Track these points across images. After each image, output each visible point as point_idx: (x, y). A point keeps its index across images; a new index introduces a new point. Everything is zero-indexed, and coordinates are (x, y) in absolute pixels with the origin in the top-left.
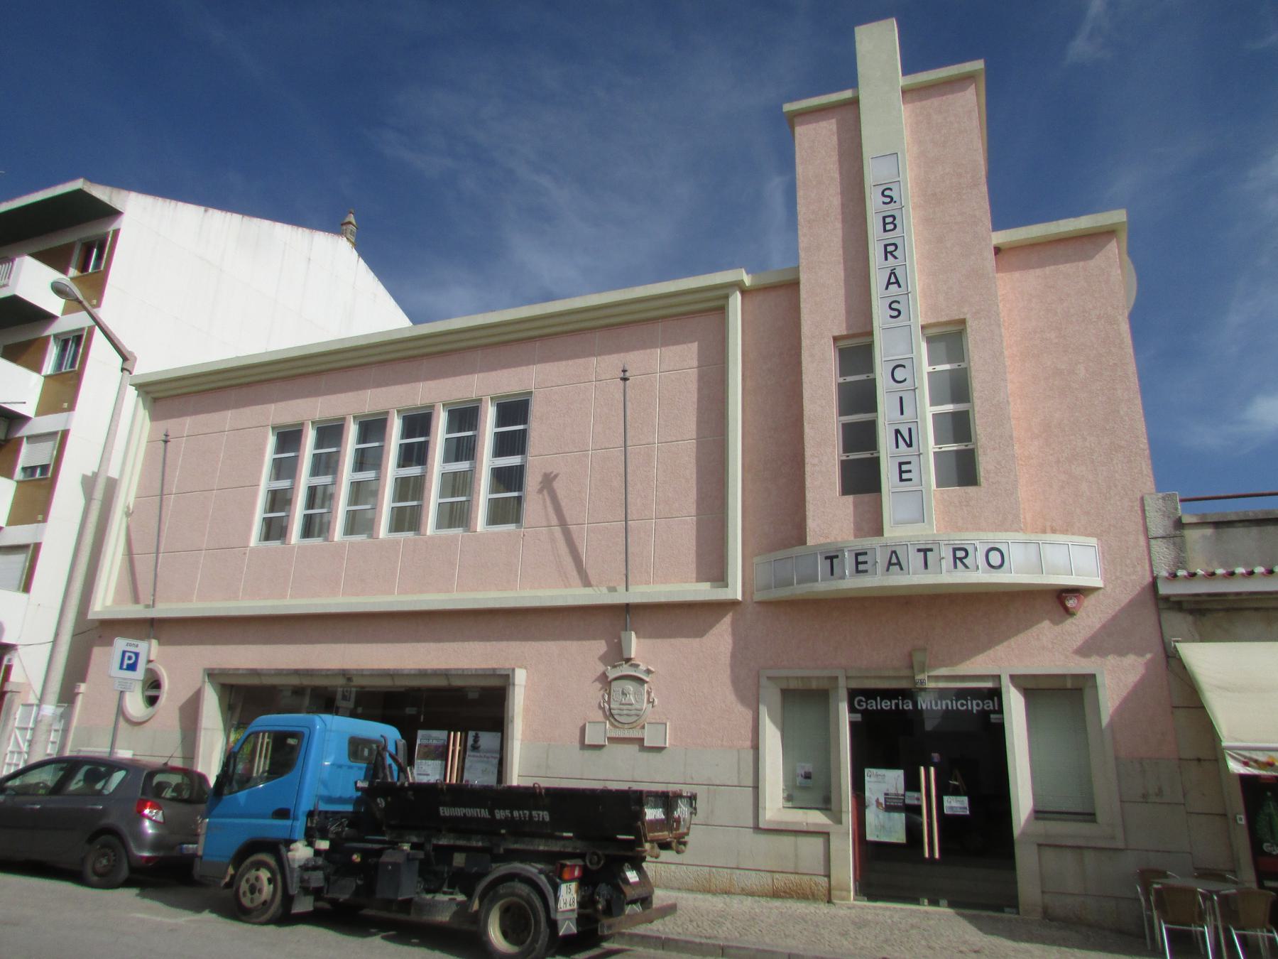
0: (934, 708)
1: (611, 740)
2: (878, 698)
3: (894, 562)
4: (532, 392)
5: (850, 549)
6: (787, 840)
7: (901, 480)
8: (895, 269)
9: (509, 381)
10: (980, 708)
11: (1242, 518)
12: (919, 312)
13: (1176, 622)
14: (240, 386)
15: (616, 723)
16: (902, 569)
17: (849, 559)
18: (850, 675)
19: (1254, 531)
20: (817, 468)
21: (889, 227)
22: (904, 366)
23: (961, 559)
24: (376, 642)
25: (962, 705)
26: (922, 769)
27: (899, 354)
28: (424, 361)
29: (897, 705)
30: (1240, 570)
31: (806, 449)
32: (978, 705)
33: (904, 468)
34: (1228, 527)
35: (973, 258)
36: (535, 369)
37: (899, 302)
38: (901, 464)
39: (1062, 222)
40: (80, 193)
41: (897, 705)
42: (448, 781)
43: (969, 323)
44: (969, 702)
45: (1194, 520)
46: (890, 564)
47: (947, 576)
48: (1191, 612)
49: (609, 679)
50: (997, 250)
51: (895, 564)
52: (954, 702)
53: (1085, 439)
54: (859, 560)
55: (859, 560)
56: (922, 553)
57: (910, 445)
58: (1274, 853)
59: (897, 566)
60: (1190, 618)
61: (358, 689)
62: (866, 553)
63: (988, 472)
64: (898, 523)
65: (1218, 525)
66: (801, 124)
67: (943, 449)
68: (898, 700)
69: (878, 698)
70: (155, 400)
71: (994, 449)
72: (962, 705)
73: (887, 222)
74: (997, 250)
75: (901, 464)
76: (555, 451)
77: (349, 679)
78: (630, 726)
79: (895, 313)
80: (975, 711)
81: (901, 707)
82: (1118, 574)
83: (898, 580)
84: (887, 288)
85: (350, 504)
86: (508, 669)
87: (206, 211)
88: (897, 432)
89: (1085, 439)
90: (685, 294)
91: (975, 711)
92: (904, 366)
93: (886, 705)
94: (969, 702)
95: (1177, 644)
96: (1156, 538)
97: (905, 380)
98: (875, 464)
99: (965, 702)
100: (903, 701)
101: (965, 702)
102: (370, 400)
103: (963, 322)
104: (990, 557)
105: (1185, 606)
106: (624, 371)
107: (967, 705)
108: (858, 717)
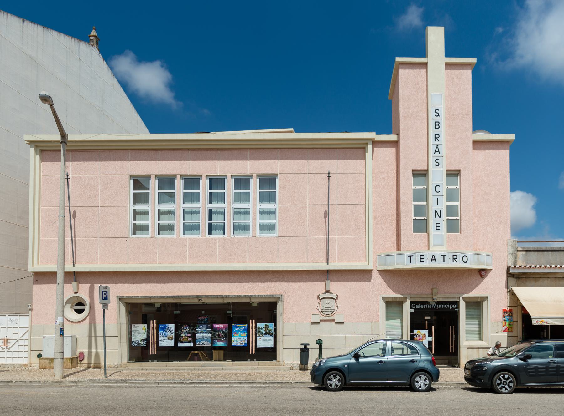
1: (321, 320)
2: (420, 304)
3: (434, 259)
4: (278, 175)
5: (418, 253)
8: (438, 145)
10: (452, 307)
11: (534, 249)
13: (512, 281)
14: (104, 150)
16: (436, 262)
19: (536, 253)
20: (405, 222)
22: (439, 186)
23: (455, 259)
24: (208, 282)
25: (446, 306)
27: (437, 182)
28: (219, 152)
29: (426, 306)
30: (533, 266)
31: (401, 214)
33: (438, 225)
34: (529, 252)
35: (465, 145)
36: (279, 162)
37: (439, 160)
41: (426, 306)
43: (461, 172)
44: (449, 305)
45: (521, 249)
46: (432, 260)
47: (449, 264)
48: (516, 278)
49: (320, 299)
51: (433, 260)
52: (444, 305)
53: (492, 219)
54: (421, 258)
55: (421, 258)
56: (443, 256)
57: (440, 217)
59: (435, 261)
60: (515, 280)
61: (458, 311)
62: (423, 256)
63: (464, 229)
64: (434, 245)
65: (527, 251)
66: (403, 68)
67: (449, 219)
68: (448, 305)
69: (420, 304)
70: (42, 151)
71: (467, 221)
72: (446, 306)
73: (436, 124)
76: (291, 204)
77: (201, 300)
78: (329, 315)
79: (437, 164)
80: (450, 308)
81: (427, 307)
82: (497, 265)
83: (434, 265)
84: (435, 153)
86: (279, 295)
87: (23, 21)
88: (436, 211)
89: (492, 219)
91: (450, 308)
92: (439, 186)
93: (422, 306)
94: (449, 305)
95: (512, 288)
96: (509, 254)
97: (439, 192)
98: (426, 222)
99: (447, 305)
100: (428, 305)
101: (447, 305)
103: (459, 171)
105: (515, 276)
106: (329, 173)
107: (448, 306)
108: (413, 310)
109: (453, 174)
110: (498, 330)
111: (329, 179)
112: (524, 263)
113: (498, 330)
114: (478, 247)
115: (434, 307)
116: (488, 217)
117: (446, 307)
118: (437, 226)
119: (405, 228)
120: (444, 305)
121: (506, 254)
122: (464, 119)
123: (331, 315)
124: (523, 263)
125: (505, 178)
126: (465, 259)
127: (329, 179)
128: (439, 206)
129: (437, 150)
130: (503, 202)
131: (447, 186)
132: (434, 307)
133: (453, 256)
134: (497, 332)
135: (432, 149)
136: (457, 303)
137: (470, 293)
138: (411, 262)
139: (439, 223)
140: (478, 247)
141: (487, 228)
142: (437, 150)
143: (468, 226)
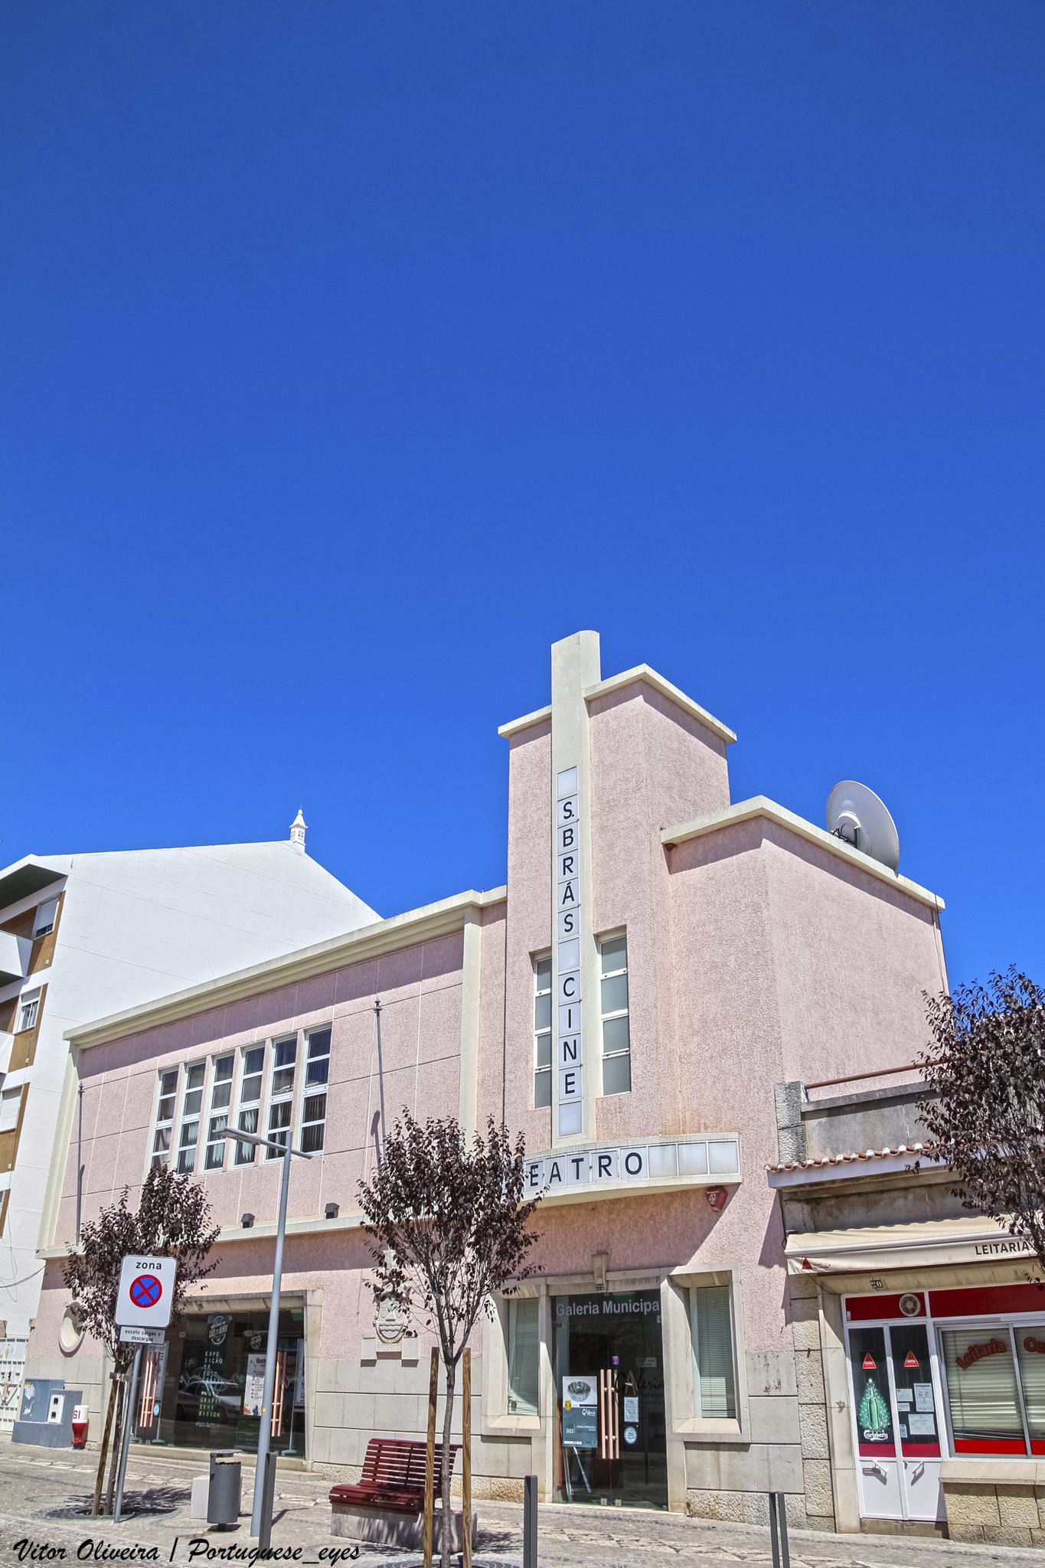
0: (615, 1312)
2: (574, 1304)
6: (502, 1447)
7: (567, 1092)
9: (314, 1018)
12: (589, 923)
15: (383, 1339)
17: (592, 1160)
18: (591, 1275)
20: (513, 1084)
21: (568, 841)
23: (605, 1167)
25: (636, 1307)
26: (602, 1371)
29: (588, 1310)
32: (648, 1307)
38: (567, 1076)
39: (430, 906)
40: (29, 867)
41: (588, 1310)
42: (141, 1425)
50: (669, 847)
52: (630, 1305)
58: (872, 1440)
69: (574, 1304)
72: (636, 1307)
74: (669, 847)
75: (567, 1076)
77: (201, 1306)
78: (393, 1341)
80: (646, 1313)
85: (307, 1119)
88: (566, 1044)
90: (350, 947)
91: (646, 1313)
102: (236, 1042)
103: (624, 927)
104: (629, 1160)
107: (640, 1307)
109: (613, 943)
110: (767, 1381)
111: (378, 1015)
112: (828, 1150)
113: (767, 1381)
114: (702, 1121)
115: (608, 1312)
116: (723, 1031)
117: (635, 1311)
118: (568, 1081)
119: (513, 1099)
120: (630, 1305)
121: (774, 1129)
122: (630, 802)
123: (397, 1339)
124: (823, 1151)
125: (758, 913)
126: (633, 1164)
127: (378, 1015)
128: (574, 1029)
129: (569, 895)
130: (757, 979)
131: (603, 973)
132: (608, 1312)
133: (601, 1158)
134: (767, 1390)
135: (559, 892)
136: (655, 1295)
137: (691, 1262)
138: (578, 1178)
139: (573, 1075)
140: (702, 1121)
141: (723, 1061)
142: (569, 894)
143: (645, 1068)
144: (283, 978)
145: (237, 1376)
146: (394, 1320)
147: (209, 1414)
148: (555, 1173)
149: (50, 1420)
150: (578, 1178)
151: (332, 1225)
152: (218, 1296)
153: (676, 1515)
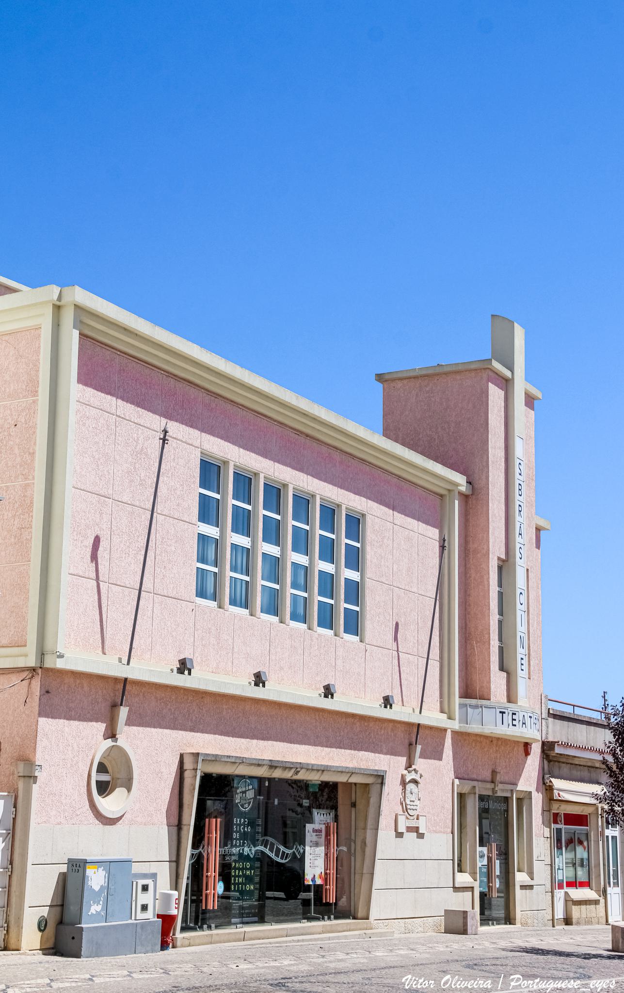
39: (282, 389)
138: (503, 724)
144: (336, 439)
145: (298, 847)
146: (413, 801)
147: (242, 887)
148: (524, 722)
149: (141, 916)
150: (503, 724)
151: (386, 714)
152: (322, 765)
153: (518, 925)
